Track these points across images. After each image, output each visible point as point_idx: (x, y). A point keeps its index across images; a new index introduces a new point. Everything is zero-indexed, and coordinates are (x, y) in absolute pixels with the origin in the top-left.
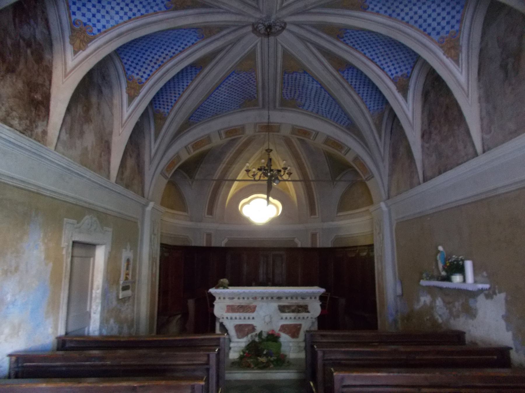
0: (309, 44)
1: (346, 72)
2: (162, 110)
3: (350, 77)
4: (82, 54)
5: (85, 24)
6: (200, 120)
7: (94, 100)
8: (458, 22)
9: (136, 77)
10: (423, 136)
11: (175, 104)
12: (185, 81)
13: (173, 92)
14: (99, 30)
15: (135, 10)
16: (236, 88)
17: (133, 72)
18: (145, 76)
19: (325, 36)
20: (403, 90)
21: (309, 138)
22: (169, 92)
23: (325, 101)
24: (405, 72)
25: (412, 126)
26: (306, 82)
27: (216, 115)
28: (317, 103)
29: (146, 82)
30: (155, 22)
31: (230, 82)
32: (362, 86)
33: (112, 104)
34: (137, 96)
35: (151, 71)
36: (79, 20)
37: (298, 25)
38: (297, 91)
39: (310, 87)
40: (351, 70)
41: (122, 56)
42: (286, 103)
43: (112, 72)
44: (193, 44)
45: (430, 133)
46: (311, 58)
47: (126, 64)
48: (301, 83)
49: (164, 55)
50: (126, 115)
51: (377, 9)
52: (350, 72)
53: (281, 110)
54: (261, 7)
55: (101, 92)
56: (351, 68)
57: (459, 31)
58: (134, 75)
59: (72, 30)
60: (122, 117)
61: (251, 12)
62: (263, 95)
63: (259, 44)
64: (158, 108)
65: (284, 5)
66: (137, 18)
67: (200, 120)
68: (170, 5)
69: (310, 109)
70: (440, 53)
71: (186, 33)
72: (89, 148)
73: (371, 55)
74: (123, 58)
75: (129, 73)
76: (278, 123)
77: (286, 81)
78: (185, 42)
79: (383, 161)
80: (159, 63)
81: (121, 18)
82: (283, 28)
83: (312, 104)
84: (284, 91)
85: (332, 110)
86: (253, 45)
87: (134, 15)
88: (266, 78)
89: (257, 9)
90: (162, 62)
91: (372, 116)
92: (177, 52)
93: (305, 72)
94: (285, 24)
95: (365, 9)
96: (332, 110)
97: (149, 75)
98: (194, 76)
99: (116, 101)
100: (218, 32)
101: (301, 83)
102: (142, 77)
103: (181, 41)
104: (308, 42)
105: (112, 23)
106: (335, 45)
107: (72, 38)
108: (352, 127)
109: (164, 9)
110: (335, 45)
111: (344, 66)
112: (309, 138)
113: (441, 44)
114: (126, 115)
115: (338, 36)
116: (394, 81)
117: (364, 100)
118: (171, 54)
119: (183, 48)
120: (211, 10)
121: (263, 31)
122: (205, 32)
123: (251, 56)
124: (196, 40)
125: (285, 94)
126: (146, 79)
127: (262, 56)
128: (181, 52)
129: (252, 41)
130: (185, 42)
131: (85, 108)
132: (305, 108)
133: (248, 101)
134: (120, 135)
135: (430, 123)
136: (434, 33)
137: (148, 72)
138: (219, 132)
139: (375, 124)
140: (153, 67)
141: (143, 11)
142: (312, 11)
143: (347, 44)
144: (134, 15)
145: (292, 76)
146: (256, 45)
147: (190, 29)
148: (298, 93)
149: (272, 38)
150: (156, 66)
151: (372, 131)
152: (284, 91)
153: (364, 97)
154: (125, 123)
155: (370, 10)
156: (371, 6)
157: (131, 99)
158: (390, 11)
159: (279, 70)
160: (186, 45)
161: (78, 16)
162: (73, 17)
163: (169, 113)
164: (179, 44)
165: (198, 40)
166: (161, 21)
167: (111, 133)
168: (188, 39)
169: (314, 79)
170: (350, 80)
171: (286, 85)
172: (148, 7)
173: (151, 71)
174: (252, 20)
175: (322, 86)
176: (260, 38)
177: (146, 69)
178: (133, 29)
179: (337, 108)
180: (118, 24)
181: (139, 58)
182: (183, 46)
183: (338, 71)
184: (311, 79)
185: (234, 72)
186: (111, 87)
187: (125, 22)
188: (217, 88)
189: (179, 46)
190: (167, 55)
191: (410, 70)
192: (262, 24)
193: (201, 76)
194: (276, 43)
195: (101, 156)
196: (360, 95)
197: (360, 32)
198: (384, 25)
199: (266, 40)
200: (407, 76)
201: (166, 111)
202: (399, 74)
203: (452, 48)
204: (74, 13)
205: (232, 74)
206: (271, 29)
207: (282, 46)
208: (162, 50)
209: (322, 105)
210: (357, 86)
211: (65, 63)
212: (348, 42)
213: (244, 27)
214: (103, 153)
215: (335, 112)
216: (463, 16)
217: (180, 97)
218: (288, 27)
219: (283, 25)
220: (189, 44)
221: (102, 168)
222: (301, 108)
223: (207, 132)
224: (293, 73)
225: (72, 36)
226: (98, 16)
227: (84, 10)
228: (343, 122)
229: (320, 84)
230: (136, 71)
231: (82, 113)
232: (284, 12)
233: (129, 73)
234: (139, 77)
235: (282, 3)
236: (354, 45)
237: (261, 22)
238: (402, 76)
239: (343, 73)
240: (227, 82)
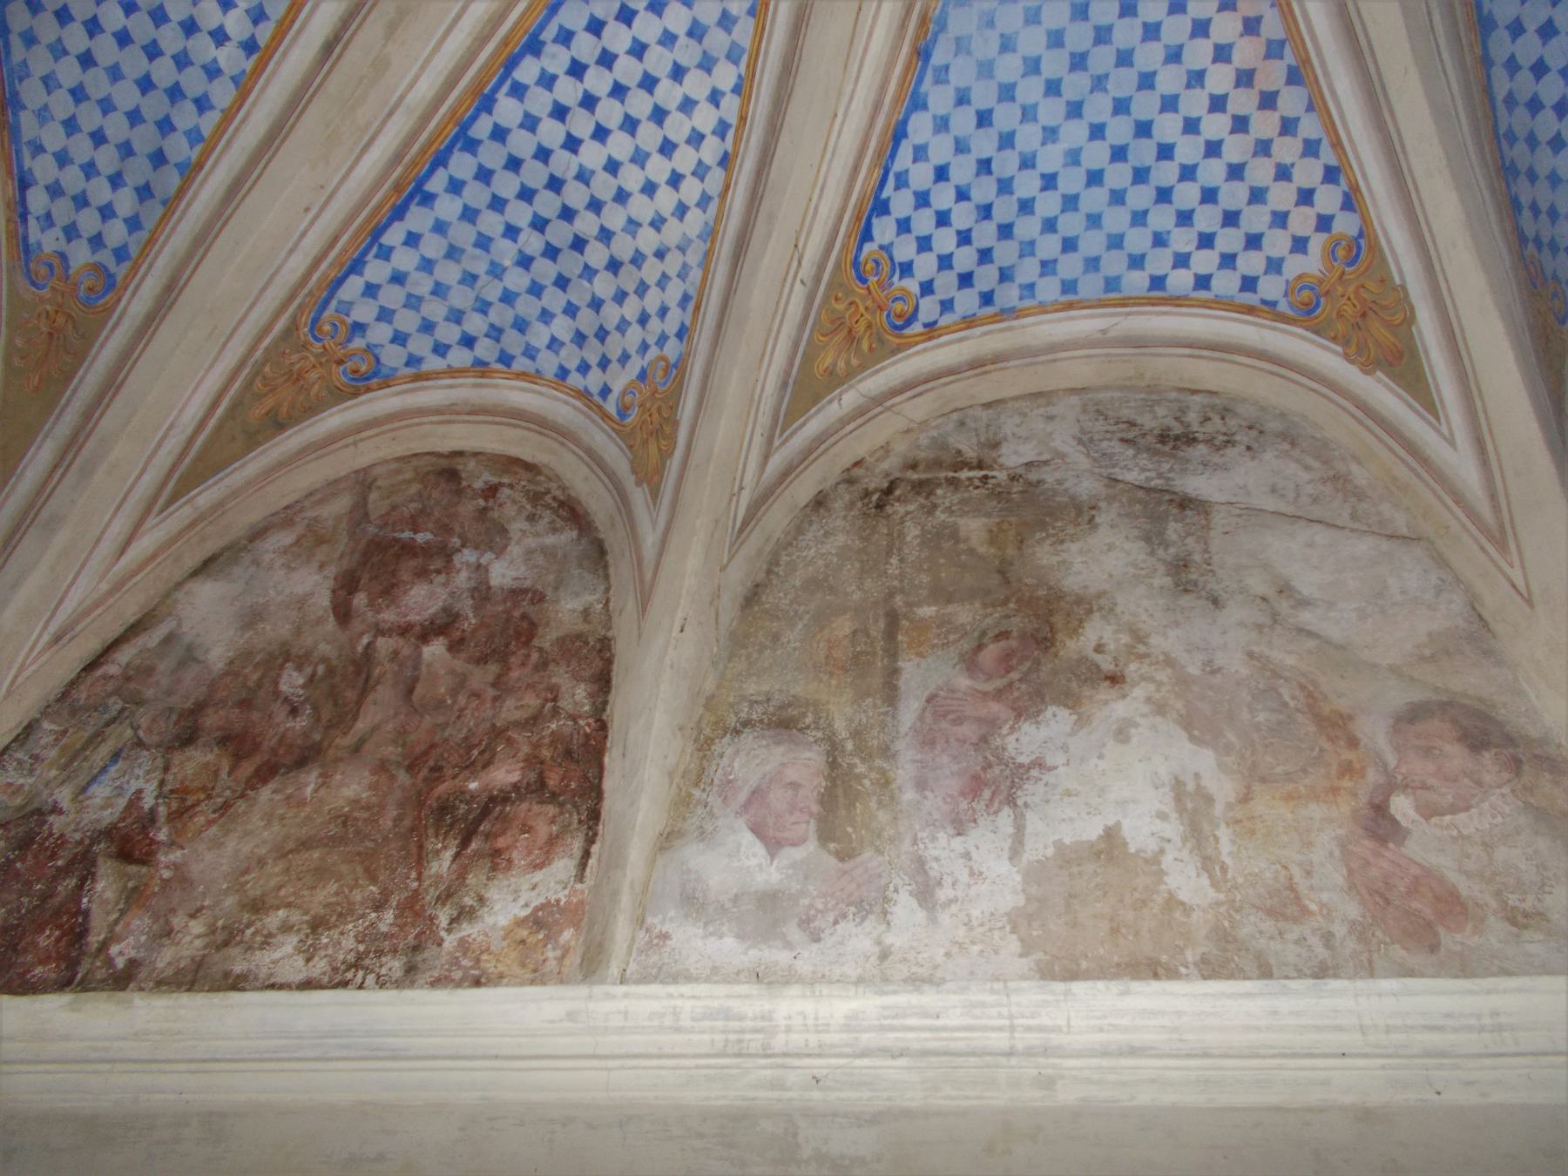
0: (648, 575)
17: (1274, 266)
29: (1365, 219)
34: (1410, 319)
60: (1459, 499)
104: (642, 581)
126: (1350, 202)
134: (1530, 602)
137: (1308, 173)
154: (1496, 508)
173: (1311, 148)
197: (696, 274)
234: (1317, 243)
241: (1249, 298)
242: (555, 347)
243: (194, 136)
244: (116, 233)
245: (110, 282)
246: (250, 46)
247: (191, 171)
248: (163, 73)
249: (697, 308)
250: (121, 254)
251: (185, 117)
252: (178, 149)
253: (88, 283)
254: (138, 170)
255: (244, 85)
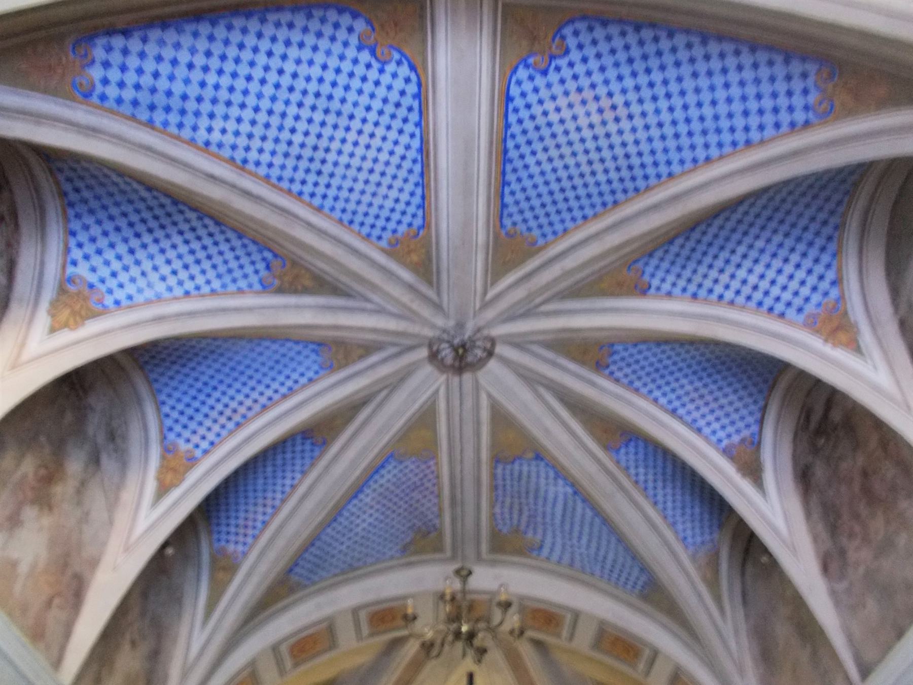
0: (542, 390)
1: (623, 451)
2: (231, 547)
3: (632, 464)
4: (66, 336)
5: (91, 286)
6: (316, 578)
7: (75, 465)
8: (833, 283)
9: (183, 446)
10: (825, 568)
11: (262, 531)
12: (289, 475)
13: (260, 501)
14: (117, 303)
15: (200, 280)
16: (395, 499)
17: (179, 435)
18: (205, 445)
19: (572, 366)
20: (752, 470)
21: (558, 635)
22: (251, 501)
23: (586, 530)
24: (746, 433)
25: (794, 550)
26: (543, 481)
27: (351, 570)
28: (567, 536)
30: (237, 310)
31: (383, 481)
32: (660, 484)
33: (117, 499)
35: (218, 435)
36: (80, 277)
37: (519, 343)
38: (526, 508)
39: (551, 496)
40: (632, 444)
41: (163, 397)
42: (506, 544)
43: (135, 434)
44: (311, 380)
45: (842, 553)
46: (549, 422)
47: (167, 416)
48: (532, 486)
49: (248, 402)
50: (142, 524)
51: (666, 286)
52: (632, 449)
53: (493, 563)
54: (445, 305)
55: (95, 460)
56: (630, 440)
57: (841, 298)
58: (181, 444)
59: (62, 290)
61: (426, 312)
62: (454, 520)
63: (442, 392)
64: (223, 543)
65: (490, 295)
66: (203, 296)
67: (316, 578)
68: (270, 280)
69: (555, 556)
70: (817, 342)
71: (299, 353)
72: (23, 568)
73: (670, 402)
74: (163, 403)
75: (171, 436)
76: (485, 592)
77: (500, 482)
78: (295, 376)
79: (741, 671)
80: (237, 418)
81: (170, 289)
82: (490, 354)
83: (559, 540)
84: (497, 510)
85: (602, 553)
86: (429, 393)
87: (198, 288)
88: (458, 476)
89: (438, 307)
90: (244, 416)
91: (693, 558)
92: (276, 397)
93: (538, 457)
94: (493, 341)
95: (643, 291)
96: (602, 553)
97: (212, 444)
98: (307, 461)
99: (128, 495)
100: (361, 357)
101: (532, 486)
102: (197, 446)
103: (287, 372)
105: (149, 294)
106: (593, 384)
107: (55, 306)
108: (654, 594)
109: (257, 287)
110: (593, 384)
111: (617, 434)
112: (558, 635)
113: (812, 325)
114: (142, 524)
115: (597, 363)
116: (727, 452)
117: (671, 520)
118: (263, 400)
119: (290, 389)
120: (350, 303)
121: (449, 360)
122: (337, 351)
123: (425, 418)
124: (316, 373)
125: (499, 517)
127: (448, 419)
128: (285, 396)
129: (428, 382)
130: (295, 376)
131: (43, 472)
132: (546, 551)
133: (422, 541)
135: (834, 529)
136: (791, 313)
137: (211, 436)
138: (355, 611)
139: (705, 579)
140: (223, 427)
141: (216, 284)
142: (545, 308)
143: (617, 381)
144: (198, 288)
145: (512, 470)
146: (437, 392)
147: (306, 343)
148: (526, 514)
149: (467, 377)
150: (230, 425)
151: (699, 595)
152: (497, 510)
153: (670, 512)
155: (652, 290)
156: (655, 282)
157: (163, 490)
158: (692, 288)
159: (485, 455)
160: (296, 382)
161: (82, 270)
162: (70, 270)
163: (245, 554)
164: (281, 378)
165: (322, 373)
166: (250, 309)
167: (94, 563)
168: (301, 369)
169: (560, 473)
170: (632, 471)
171: (500, 492)
172: (227, 279)
174: (429, 333)
175: (578, 491)
176: (443, 378)
177: (209, 429)
178: (192, 314)
179: (612, 546)
180: (159, 298)
181: (196, 404)
182: (289, 383)
183: (606, 448)
184: (552, 474)
185: (392, 456)
186: (124, 465)
187: (176, 298)
188: (356, 496)
189: (282, 384)
190: (256, 401)
191: (755, 428)
192: (448, 342)
193: (323, 463)
194: (477, 387)
195: (49, 604)
196: (660, 506)
198: (683, 315)
199: (456, 380)
200: (752, 443)
201: (240, 548)
202: (736, 439)
203: (837, 327)
204: (74, 263)
205: (387, 461)
206: (465, 350)
207: (489, 396)
208: (246, 390)
209: (579, 542)
210: (650, 485)
211: (23, 345)
212: (619, 374)
213: (411, 348)
214: (57, 601)
215: (611, 556)
216: (839, 270)
217: (274, 515)
218: (499, 349)
219: (488, 345)
220: (303, 380)
221: (46, 635)
222: (535, 554)
223: (327, 611)
224: (513, 463)
225: (57, 300)
226: (123, 277)
227: (96, 261)
228: (630, 583)
229: (573, 485)
230: (187, 434)
231: (31, 476)
232: (490, 314)
233: (171, 436)
235: (485, 293)
236: (631, 383)
237: (445, 336)
238: (743, 441)
239: (618, 451)
240: (376, 482)
241: (165, 431)
242: (464, 573)
243: (166, 124)
244: (112, 92)
245: (87, 95)
246: (207, 144)
247: (150, 124)
248: (191, 105)
249: (131, 307)
250: (103, 97)
251: (174, 118)
252: (159, 117)
253: (84, 82)
254: (144, 98)
255: (192, 142)
